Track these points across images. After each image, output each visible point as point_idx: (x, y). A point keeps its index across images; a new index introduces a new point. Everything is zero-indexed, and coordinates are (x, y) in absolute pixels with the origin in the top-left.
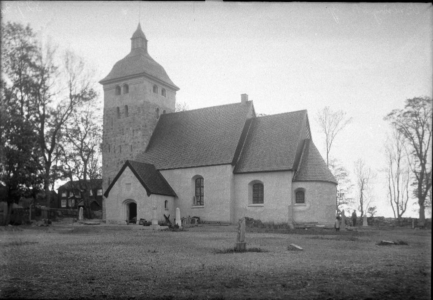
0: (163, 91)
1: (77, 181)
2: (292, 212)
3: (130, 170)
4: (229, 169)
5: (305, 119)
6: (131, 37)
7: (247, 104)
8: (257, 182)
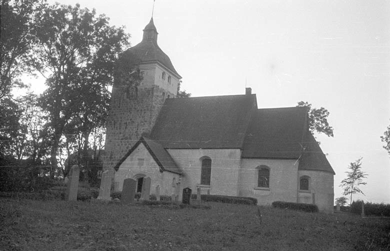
0: (169, 77)
1: (106, 136)
2: (298, 198)
3: (143, 146)
4: (238, 152)
5: (306, 116)
6: (144, 28)
7: (249, 99)
8: (267, 168)
